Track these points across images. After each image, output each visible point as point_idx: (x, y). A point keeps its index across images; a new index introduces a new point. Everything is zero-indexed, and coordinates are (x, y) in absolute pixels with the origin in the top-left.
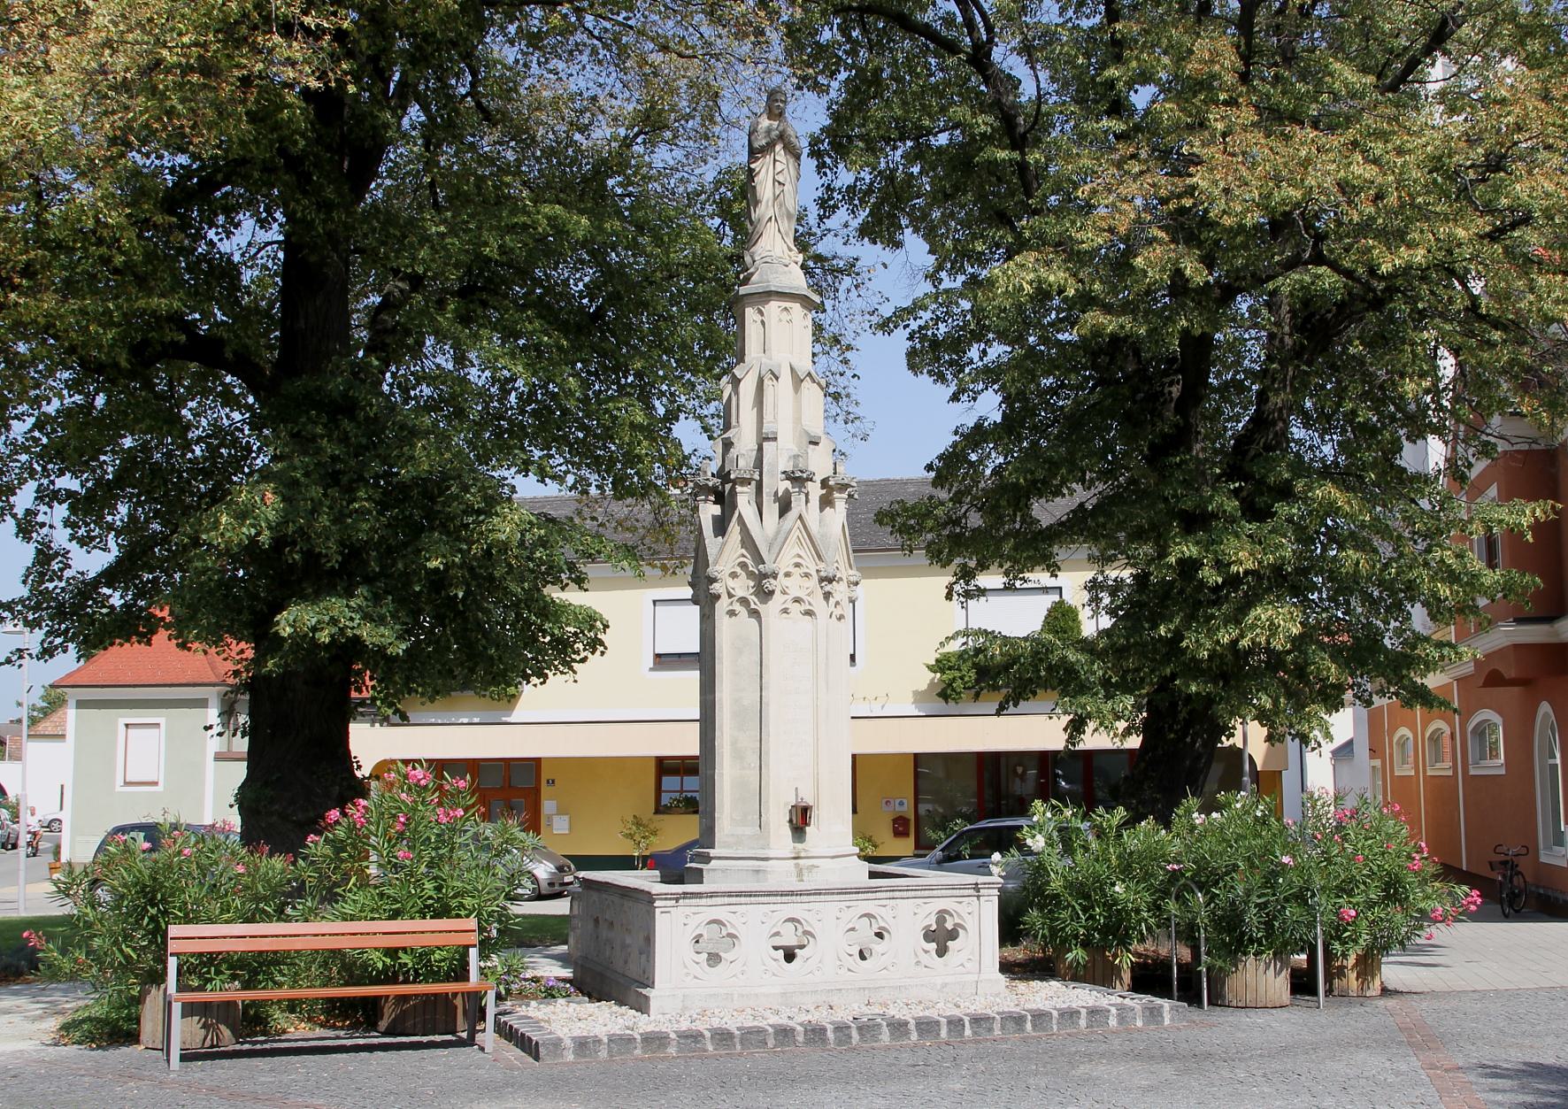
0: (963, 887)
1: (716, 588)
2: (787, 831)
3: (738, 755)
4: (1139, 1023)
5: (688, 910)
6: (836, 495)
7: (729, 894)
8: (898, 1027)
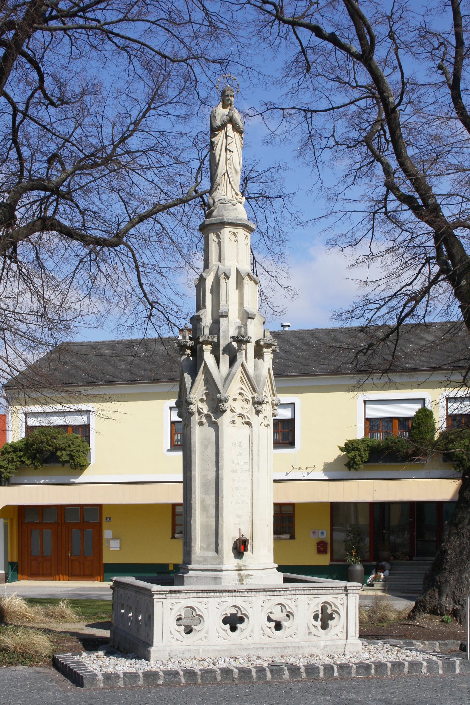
0: (339, 588)
1: (193, 408)
2: (232, 555)
3: (204, 508)
4: (441, 672)
5: (173, 601)
6: (265, 350)
7: (198, 591)
8: (294, 670)
